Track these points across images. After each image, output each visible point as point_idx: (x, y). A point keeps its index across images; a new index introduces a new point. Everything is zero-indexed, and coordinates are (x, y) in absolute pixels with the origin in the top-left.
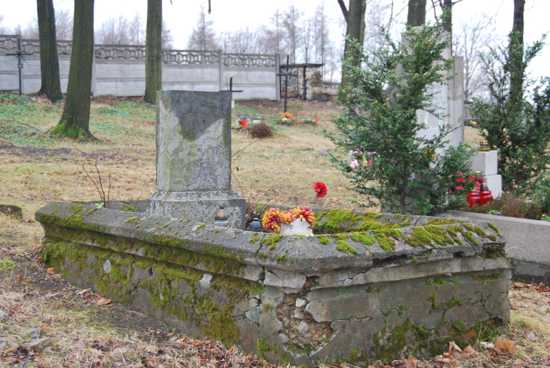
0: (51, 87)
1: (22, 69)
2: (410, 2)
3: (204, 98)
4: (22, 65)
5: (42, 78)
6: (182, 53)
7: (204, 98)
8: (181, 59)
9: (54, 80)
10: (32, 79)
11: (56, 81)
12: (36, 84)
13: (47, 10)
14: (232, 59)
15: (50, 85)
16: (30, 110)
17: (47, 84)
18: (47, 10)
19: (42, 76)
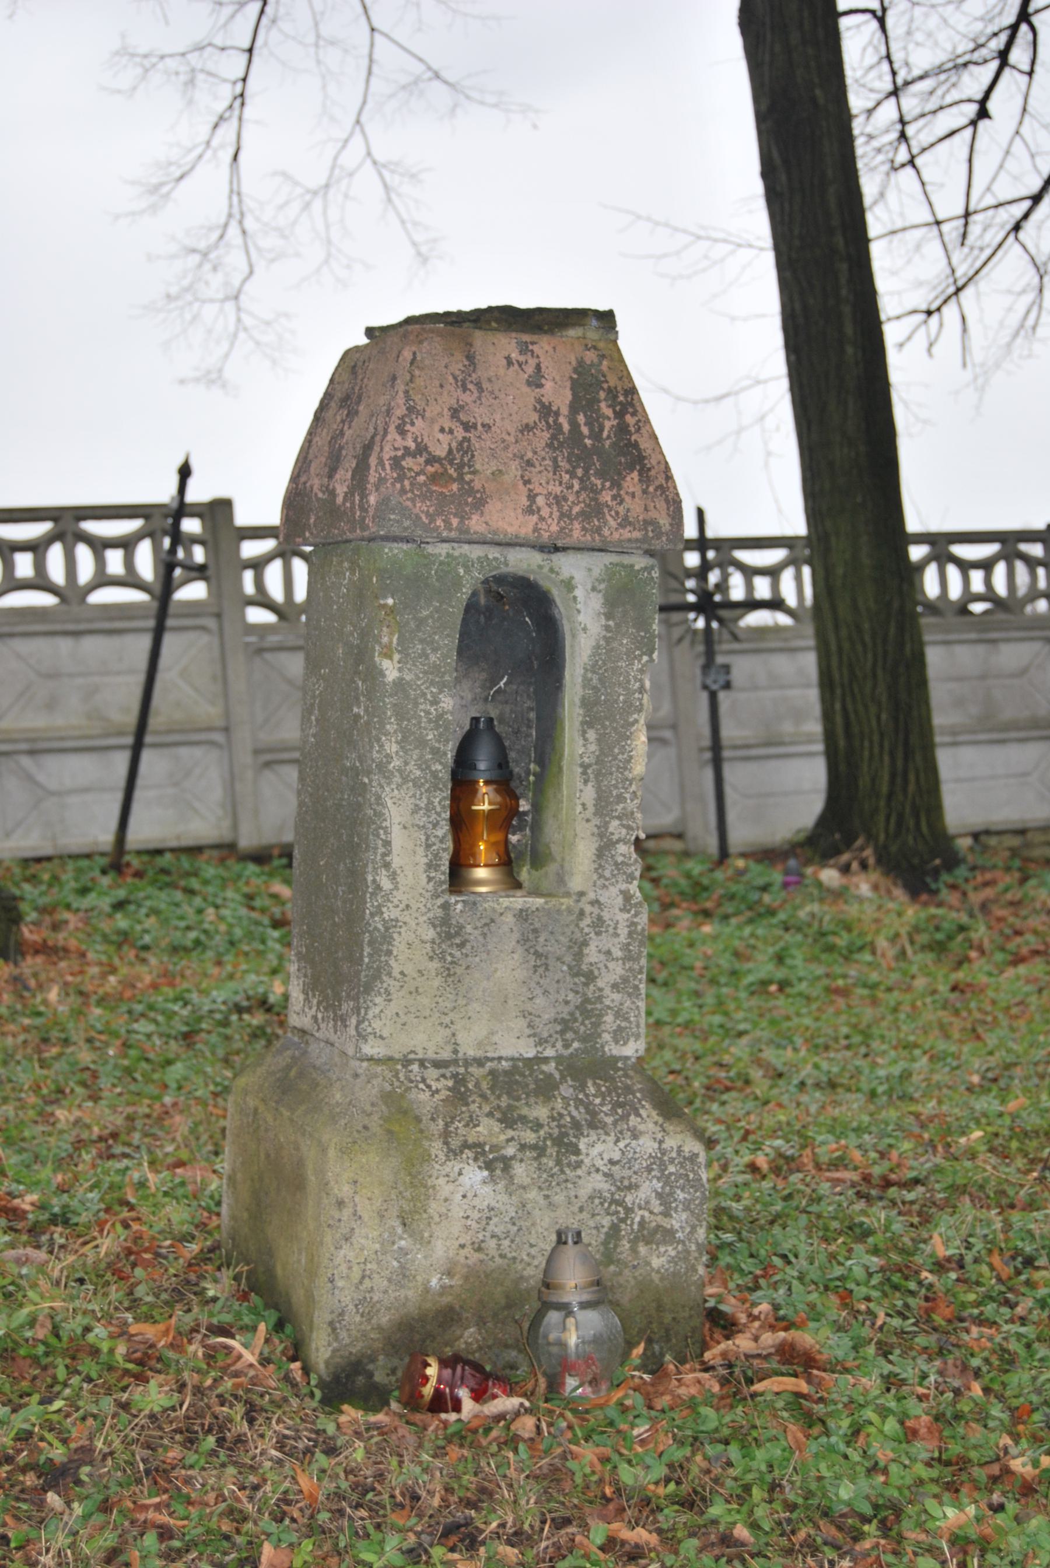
0: (890, 795)
1: (722, 695)
2: (750, 21)
3: (1015, 841)
4: (727, 668)
5: (832, 755)
6: (746, 556)
7: (1015, 841)
8: (86, 571)
9: (908, 755)
10: (752, 767)
11: (918, 758)
12: (792, 790)
13: (849, 330)
14: (99, 546)
15: (885, 789)
16: (830, 949)
17: (864, 781)
18: (849, 330)
19: (829, 736)
